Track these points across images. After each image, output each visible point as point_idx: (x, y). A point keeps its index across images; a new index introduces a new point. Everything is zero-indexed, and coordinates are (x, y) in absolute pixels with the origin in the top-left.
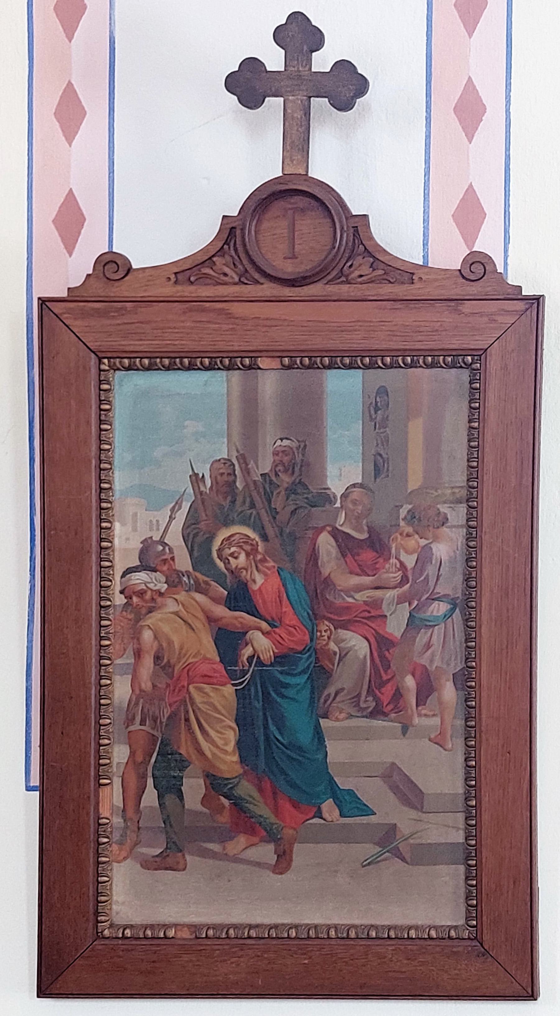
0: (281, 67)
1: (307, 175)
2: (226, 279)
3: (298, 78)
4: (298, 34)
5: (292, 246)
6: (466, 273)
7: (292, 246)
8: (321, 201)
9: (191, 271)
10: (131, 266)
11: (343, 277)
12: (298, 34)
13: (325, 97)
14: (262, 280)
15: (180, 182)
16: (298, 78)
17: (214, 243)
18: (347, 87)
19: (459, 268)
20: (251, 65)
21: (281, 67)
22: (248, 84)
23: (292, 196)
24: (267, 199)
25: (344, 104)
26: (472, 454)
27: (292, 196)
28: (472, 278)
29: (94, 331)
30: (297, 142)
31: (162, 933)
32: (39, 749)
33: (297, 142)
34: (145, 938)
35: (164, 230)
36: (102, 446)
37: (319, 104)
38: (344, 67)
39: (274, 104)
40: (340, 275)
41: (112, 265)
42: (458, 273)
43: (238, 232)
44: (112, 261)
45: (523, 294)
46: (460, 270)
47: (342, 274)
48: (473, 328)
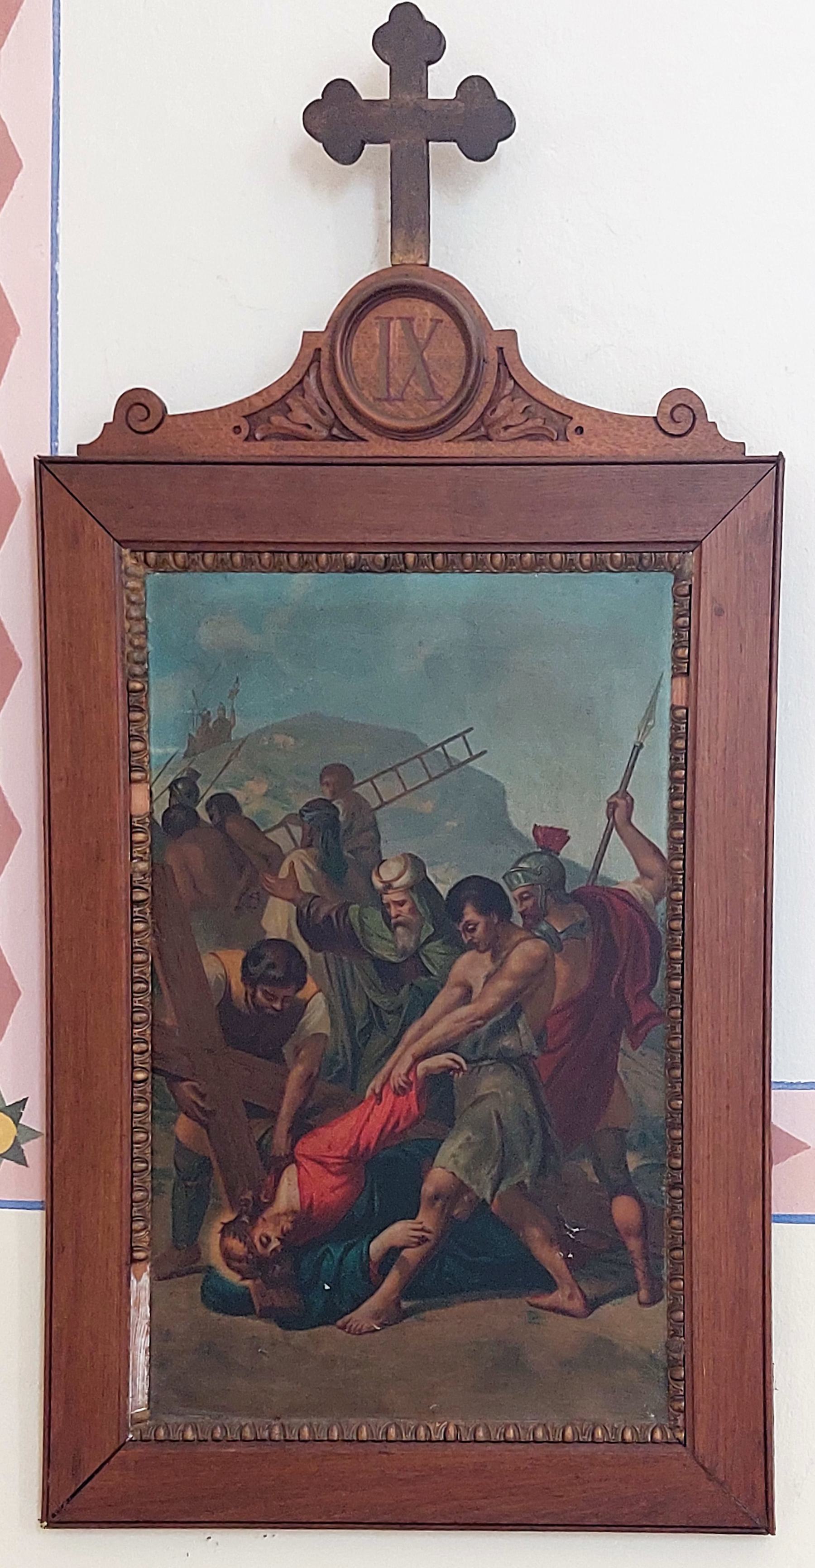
0: (385, 94)
1: (427, 265)
2: (309, 432)
3: (405, 120)
4: (408, 40)
5: (402, 440)
7: (402, 440)
8: (448, 302)
9: (256, 416)
10: (165, 410)
11: (483, 431)
12: (408, 40)
13: (455, 141)
15: (208, 287)
16: (405, 120)
18: (482, 122)
19: (655, 415)
20: (339, 91)
21: (385, 94)
22: (338, 122)
23: (402, 294)
24: (363, 305)
25: (481, 151)
27: (402, 294)
29: (135, 497)
30: (409, 216)
32: (774, 1361)
33: (409, 216)
37: (444, 154)
38: (476, 87)
39: (377, 154)
40: (479, 423)
41: (137, 407)
42: (652, 422)
44: (146, 408)
45: (747, 454)
46: (655, 418)
47: (483, 423)
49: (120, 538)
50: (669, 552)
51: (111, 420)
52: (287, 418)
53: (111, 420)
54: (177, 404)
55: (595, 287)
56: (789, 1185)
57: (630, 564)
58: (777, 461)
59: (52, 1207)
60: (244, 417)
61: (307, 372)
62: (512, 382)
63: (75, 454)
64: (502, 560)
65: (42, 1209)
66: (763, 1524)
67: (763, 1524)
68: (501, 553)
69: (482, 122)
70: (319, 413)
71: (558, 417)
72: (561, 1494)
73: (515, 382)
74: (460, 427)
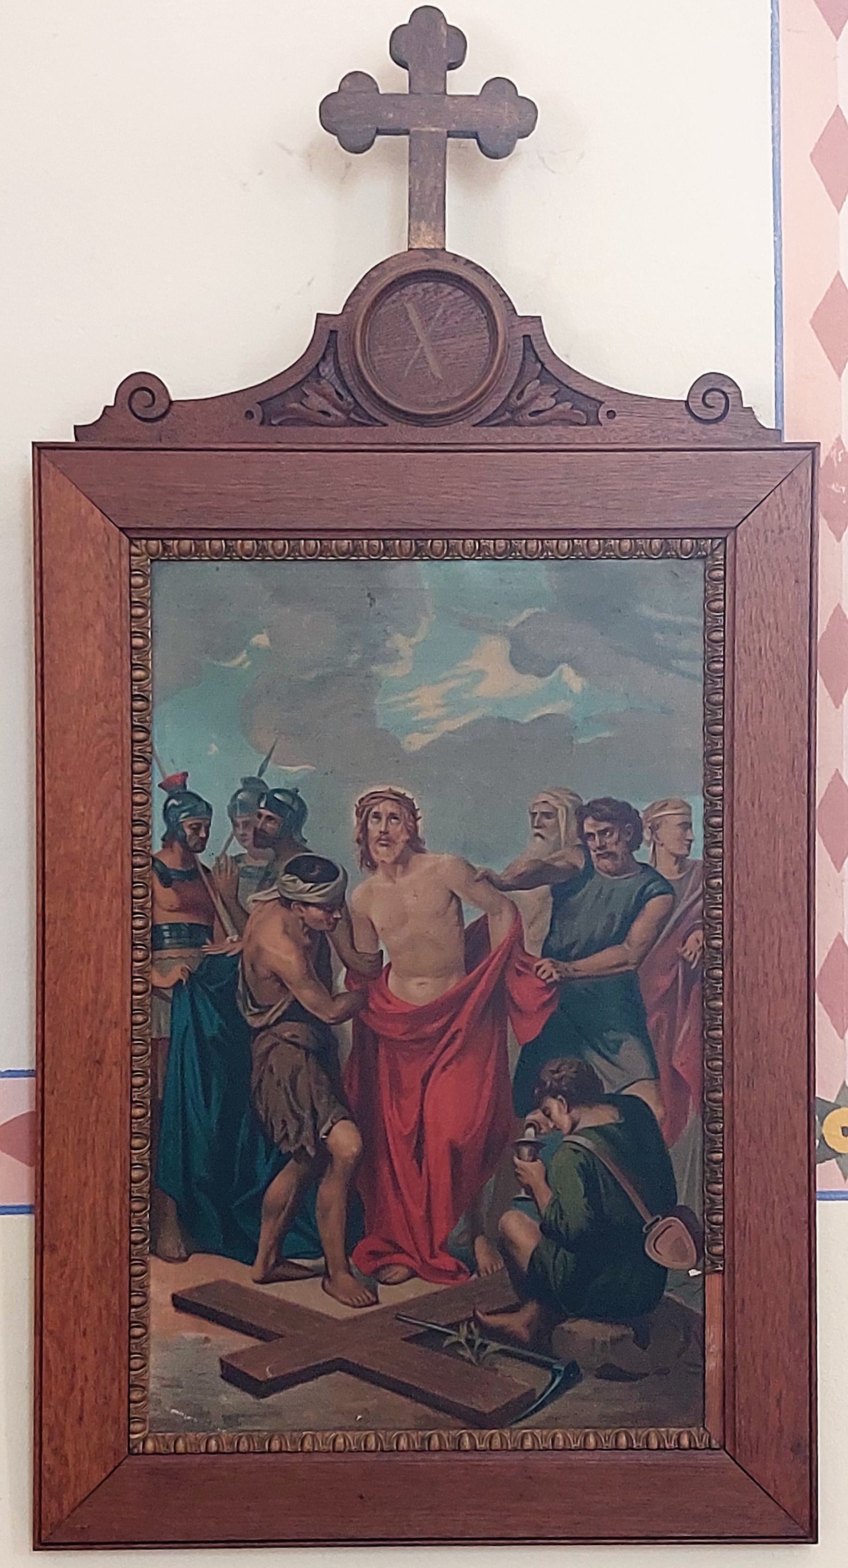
1: (444, 249)
3: (421, 110)
4: (428, 43)
5: (415, 403)
6: (696, 405)
7: (415, 403)
8: (469, 289)
9: (270, 407)
12: (428, 43)
14: (384, 418)
15: (237, 292)
16: (421, 110)
17: (352, 300)
18: (502, 122)
19: (685, 399)
22: (352, 116)
24: (387, 290)
25: (496, 149)
26: (714, 713)
28: (718, 413)
30: (426, 205)
31: (137, 600)
33: (426, 205)
34: (175, 1453)
35: (232, 338)
36: (133, 581)
41: (141, 393)
42: (684, 405)
43: (341, 337)
44: (153, 395)
46: (171, 402)
48: (683, 503)
49: (120, 526)
50: (242, 540)
51: (112, 404)
52: (302, 404)
53: (112, 404)
54: (181, 388)
55: (640, 269)
56: (829, 1175)
57: (700, 550)
58: (813, 448)
59: (40, 1209)
60: (259, 403)
61: (324, 358)
62: (539, 366)
63: (73, 440)
64: (569, 546)
65: (29, 1213)
66: (811, 1536)
67: (811, 1536)
68: (315, 540)
69: (502, 122)
70: (336, 396)
71: (587, 404)
72: (425, 465)
73: (543, 365)
74: (488, 409)
